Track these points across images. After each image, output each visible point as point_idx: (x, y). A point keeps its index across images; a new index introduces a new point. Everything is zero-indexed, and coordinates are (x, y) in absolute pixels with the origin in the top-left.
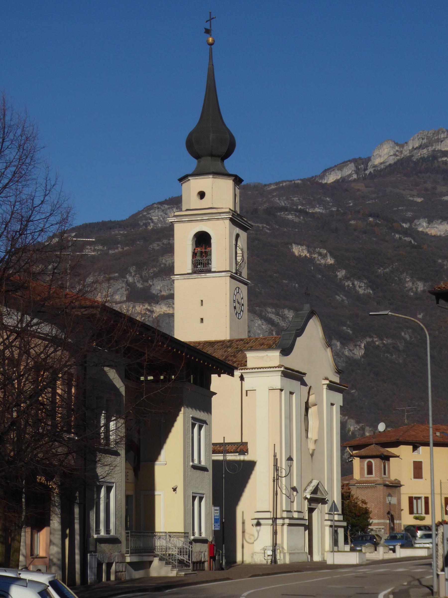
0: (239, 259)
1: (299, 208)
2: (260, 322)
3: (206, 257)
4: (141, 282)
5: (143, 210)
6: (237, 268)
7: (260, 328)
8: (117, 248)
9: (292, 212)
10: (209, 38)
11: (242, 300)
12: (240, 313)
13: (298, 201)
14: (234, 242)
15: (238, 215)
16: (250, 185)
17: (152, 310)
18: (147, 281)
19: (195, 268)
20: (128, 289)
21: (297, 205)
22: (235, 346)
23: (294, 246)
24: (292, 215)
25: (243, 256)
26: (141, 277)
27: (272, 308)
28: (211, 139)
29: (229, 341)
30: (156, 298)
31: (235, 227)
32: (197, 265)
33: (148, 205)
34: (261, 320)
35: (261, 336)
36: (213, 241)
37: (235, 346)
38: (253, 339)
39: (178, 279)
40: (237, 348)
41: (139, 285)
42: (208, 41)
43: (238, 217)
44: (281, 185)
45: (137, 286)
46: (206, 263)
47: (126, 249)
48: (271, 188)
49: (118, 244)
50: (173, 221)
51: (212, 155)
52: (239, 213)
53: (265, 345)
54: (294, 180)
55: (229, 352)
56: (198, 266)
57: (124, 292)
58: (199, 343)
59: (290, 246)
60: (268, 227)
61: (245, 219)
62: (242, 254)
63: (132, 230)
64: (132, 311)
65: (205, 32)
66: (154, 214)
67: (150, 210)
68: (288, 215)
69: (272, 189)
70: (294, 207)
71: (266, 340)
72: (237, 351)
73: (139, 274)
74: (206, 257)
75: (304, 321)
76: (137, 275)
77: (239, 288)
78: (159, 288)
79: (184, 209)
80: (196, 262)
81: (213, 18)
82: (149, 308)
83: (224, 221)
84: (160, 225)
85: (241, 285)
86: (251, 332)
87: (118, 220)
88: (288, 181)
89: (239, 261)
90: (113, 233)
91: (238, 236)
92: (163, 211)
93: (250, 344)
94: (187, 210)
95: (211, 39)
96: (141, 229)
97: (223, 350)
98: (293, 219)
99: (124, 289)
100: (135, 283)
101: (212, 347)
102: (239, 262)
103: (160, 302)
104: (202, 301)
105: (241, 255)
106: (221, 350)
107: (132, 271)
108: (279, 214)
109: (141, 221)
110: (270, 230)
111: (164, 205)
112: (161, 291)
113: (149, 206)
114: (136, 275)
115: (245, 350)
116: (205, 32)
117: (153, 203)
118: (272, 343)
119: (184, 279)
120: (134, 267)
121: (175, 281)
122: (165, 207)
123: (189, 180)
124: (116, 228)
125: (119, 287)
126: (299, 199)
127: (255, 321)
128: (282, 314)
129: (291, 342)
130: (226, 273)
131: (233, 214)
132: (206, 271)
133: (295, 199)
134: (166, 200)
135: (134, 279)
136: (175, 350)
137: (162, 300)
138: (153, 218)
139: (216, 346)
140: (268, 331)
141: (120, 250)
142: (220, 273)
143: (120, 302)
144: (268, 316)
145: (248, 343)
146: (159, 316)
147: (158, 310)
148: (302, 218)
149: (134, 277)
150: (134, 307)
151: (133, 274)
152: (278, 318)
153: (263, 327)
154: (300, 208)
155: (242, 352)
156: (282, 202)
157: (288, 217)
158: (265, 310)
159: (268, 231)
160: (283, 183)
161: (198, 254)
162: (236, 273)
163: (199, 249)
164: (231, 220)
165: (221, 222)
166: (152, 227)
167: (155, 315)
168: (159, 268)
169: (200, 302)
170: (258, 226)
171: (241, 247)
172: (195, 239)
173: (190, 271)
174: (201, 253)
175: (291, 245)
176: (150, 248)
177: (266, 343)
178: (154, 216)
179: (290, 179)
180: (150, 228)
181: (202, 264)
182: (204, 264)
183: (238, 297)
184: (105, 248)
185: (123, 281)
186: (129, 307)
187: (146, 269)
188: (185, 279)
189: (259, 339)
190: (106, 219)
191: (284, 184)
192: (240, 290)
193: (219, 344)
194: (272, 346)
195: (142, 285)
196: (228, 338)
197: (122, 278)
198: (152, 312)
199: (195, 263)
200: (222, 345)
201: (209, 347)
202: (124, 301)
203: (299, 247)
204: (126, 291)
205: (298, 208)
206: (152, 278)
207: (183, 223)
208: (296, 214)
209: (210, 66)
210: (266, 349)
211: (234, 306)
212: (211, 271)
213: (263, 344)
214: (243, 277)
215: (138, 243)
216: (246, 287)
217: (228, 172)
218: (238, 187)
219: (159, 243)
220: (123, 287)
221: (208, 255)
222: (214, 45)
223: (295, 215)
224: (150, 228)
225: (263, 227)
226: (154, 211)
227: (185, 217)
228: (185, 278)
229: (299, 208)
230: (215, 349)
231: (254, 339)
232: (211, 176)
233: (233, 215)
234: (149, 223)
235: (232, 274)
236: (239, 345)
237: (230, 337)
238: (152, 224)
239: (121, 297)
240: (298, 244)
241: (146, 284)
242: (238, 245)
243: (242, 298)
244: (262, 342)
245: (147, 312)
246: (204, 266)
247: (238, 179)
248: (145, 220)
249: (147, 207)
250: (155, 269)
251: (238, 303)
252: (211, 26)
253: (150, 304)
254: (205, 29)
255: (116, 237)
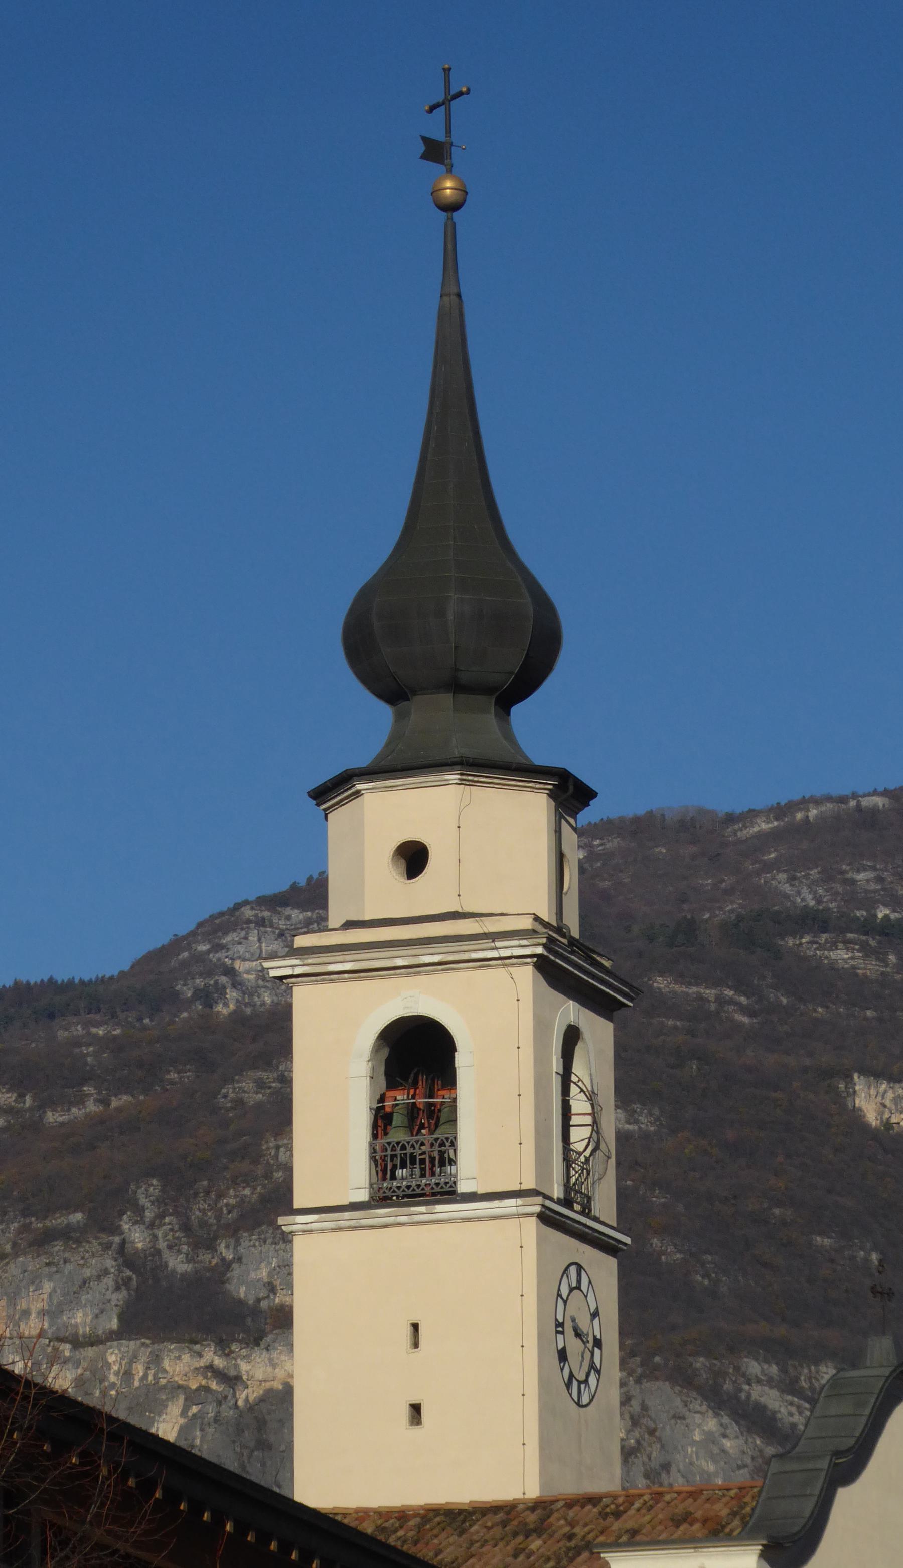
0: (580, 1136)
1: (880, 915)
2: (712, 1424)
3: (432, 1133)
4: (185, 1248)
5: (193, 934)
6: (573, 1180)
7: (716, 1450)
8: (81, 1101)
9: (850, 936)
10: (445, 178)
11: (596, 1321)
12: (586, 1382)
13: (873, 886)
14: (556, 1064)
15: (572, 942)
16: (663, 816)
17: (232, 1373)
18: (211, 1246)
19: (384, 1179)
20: (127, 1282)
21: (871, 904)
22: (561, 1527)
23: (860, 1083)
24: (847, 949)
25: (595, 1125)
26: (186, 1228)
27: (766, 1361)
28: (451, 617)
29: (537, 1505)
30: (249, 1321)
31: (561, 997)
32: (394, 1168)
33: (216, 910)
34: (717, 1415)
35: (720, 1482)
36: (460, 1060)
37: (561, 1527)
38: (641, 1496)
39: (310, 1231)
40: (570, 1537)
41: (178, 1264)
42: (436, 192)
43: (573, 952)
44: (799, 816)
45: (166, 1266)
46: (432, 1159)
47: (121, 1103)
48: (756, 829)
49: (84, 1081)
50: (288, 972)
51: (456, 687)
52: (575, 933)
53: (695, 1520)
54: (855, 796)
55: (532, 1553)
56: (399, 1172)
57: (109, 1295)
58: (402, 1515)
59: (842, 1086)
60: (743, 1000)
61: (607, 964)
62: (593, 1114)
63: (147, 1021)
64: (145, 1376)
65: (425, 156)
66: (241, 949)
67: (226, 933)
68: (834, 946)
69: (760, 835)
70: (858, 914)
71: (699, 1501)
72: (569, 1549)
73: (176, 1213)
74: (432, 1133)
75: (867, 1412)
76: (167, 1220)
77: (580, 1268)
78: (264, 1274)
79: (335, 918)
80: (389, 1152)
81: (461, 94)
82: (219, 1362)
83: (512, 970)
84: (268, 1000)
85: (587, 1254)
86: (674, 1469)
87: (86, 979)
88: (829, 799)
89: (580, 1147)
90: (62, 1034)
91: (572, 1036)
92: (282, 935)
93: (629, 1521)
94: (350, 925)
95: (449, 184)
96: (185, 1014)
97: (509, 1548)
98: (852, 962)
99: (109, 1281)
100: (158, 1252)
101: (460, 1535)
102: (580, 1154)
103: (269, 1338)
104: (415, 1327)
105: (588, 1120)
106: (501, 1545)
107: (143, 1201)
108: (790, 942)
109: (185, 980)
110: (752, 1014)
111: (288, 911)
112: (272, 1289)
113: (222, 914)
114: (161, 1216)
115: (604, 1545)
116: (425, 156)
117: (239, 900)
118: (725, 1512)
119: (334, 1230)
120: (155, 1182)
121: (298, 1241)
122: (289, 918)
123: (358, 794)
124: (76, 1013)
125: (87, 1273)
126: (880, 879)
127: (688, 1421)
128: (812, 1388)
129: (808, 1507)
130: (519, 1201)
131: (551, 939)
132: (434, 1194)
133: (861, 876)
134: (294, 887)
135: (155, 1237)
136: (273, 1546)
137: (276, 1327)
138: (238, 965)
139: (475, 1528)
140: (749, 1461)
141: (91, 1107)
142: (496, 1203)
143: (94, 1341)
144: (749, 1396)
145: (617, 1515)
146: (262, 1400)
147: (259, 1374)
148: (892, 958)
149: (151, 1226)
150: (156, 1360)
151: (149, 1215)
152: (791, 1404)
153: (727, 1444)
154: (886, 917)
155: (592, 1553)
156: (805, 891)
157: (833, 955)
158: (737, 1369)
159: (746, 1020)
160: (808, 811)
161: (397, 1120)
162: (567, 1202)
163: (401, 1097)
164: (543, 965)
165: (498, 974)
166: (232, 1006)
167: (245, 1396)
168: (264, 1186)
169: (409, 1330)
170: (700, 998)
171: (587, 1081)
172: (385, 1052)
173: (363, 1196)
174: (412, 1112)
175: (848, 1077)
176: (225, 1097)
177: (699, 1514)
178: (244, 960)
179: (838, 790)
180: (225, 1011)
181: (413, 1162)
182: (423, 1161)
183: (578, 1309)
184: (28, 1101)
185: (108, 1246)
186: (134, 1358)
187: (207, 1193)
188: (340, 1229)
189: (668, 1498)
190: (34, 975)
191: (813, 813)
192: (583, 1274)
193: (489, 1520)
194: (724, 1527)
195: (189, 1261)
196: (533, 1491)
197: (103, 1230)
198: (232, 1380)
199: (384, 1159)
200: (504, 1524)
201: (443, 1536)
202: (112, 1332)
203: (884, 1086)
204: (118, 1288)
205: (876, 916)
206: (234, 1231)
207: (333, 981)
208: (867, 942)
209: (446, 299)
210: (700, 1541)
211: (560, 1346)
212: (453, 1192)
213: (686, 1518)
214: (596, 1219)
215: (173, 1076)
216: (612, 1263)
217: (526, 758)
218: (572, 821)
219: (264, 1075)
220: (106, 1272)
221: (442, 1120)
222: (462, 209)
223: (864, 947)
224: (223, 1010)
225: (721, 1001)
226: (243, 934)
227: (338, 957)
228: (343, 1224)
229: (880, 915)
230: (472, 1543)
231: (646, 1498)
232: (453, 777)
233: (550, 945)
234: (221, 991)
235: (548, 1203)
236: (578, 1523)
237: (543, 1485)
238: (232, 995)
239: (97, 1316)
240: (876, 1074)
241: (205, 1257)
242: (574, 1078)
243: (595, 1314)
244: (680, 1509)
245: (214, 1385)
246: (423, 1170)
247: (571, 788)
248: (201, 975)
249: (213, 917)
250: (247, 1192)
251: (578, 1334)
252: (449, 131)
253: (223, 1346)
254: (425, 140)
255: (77, 1050)
